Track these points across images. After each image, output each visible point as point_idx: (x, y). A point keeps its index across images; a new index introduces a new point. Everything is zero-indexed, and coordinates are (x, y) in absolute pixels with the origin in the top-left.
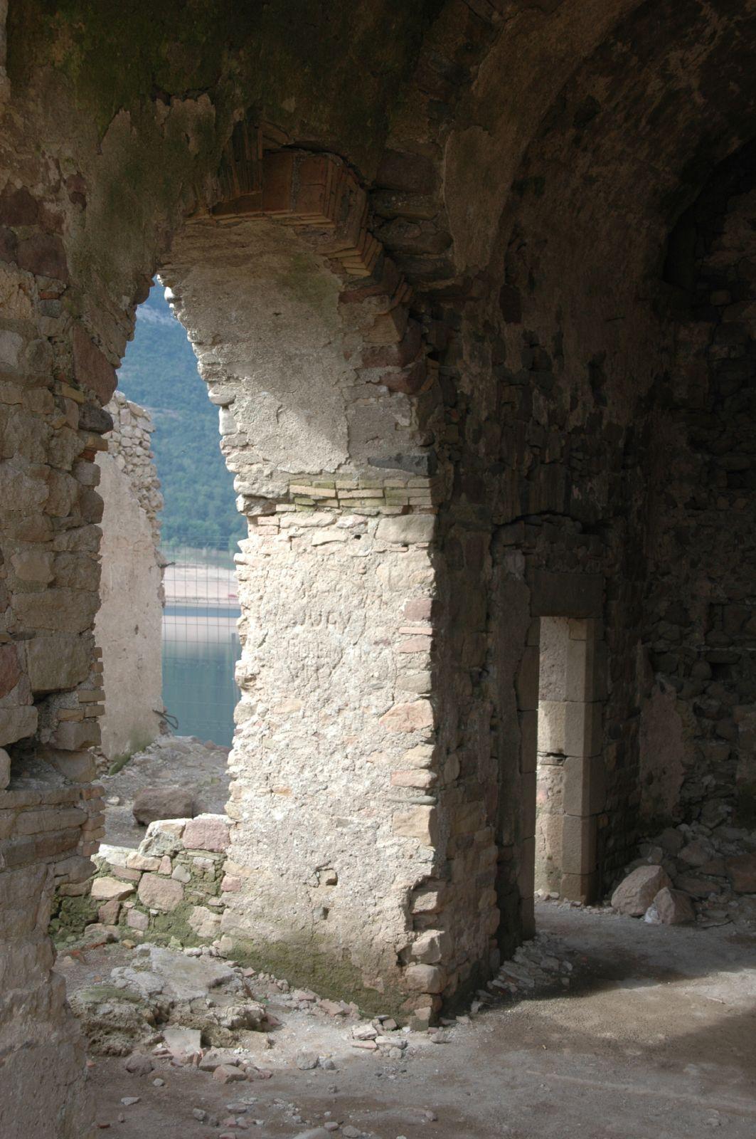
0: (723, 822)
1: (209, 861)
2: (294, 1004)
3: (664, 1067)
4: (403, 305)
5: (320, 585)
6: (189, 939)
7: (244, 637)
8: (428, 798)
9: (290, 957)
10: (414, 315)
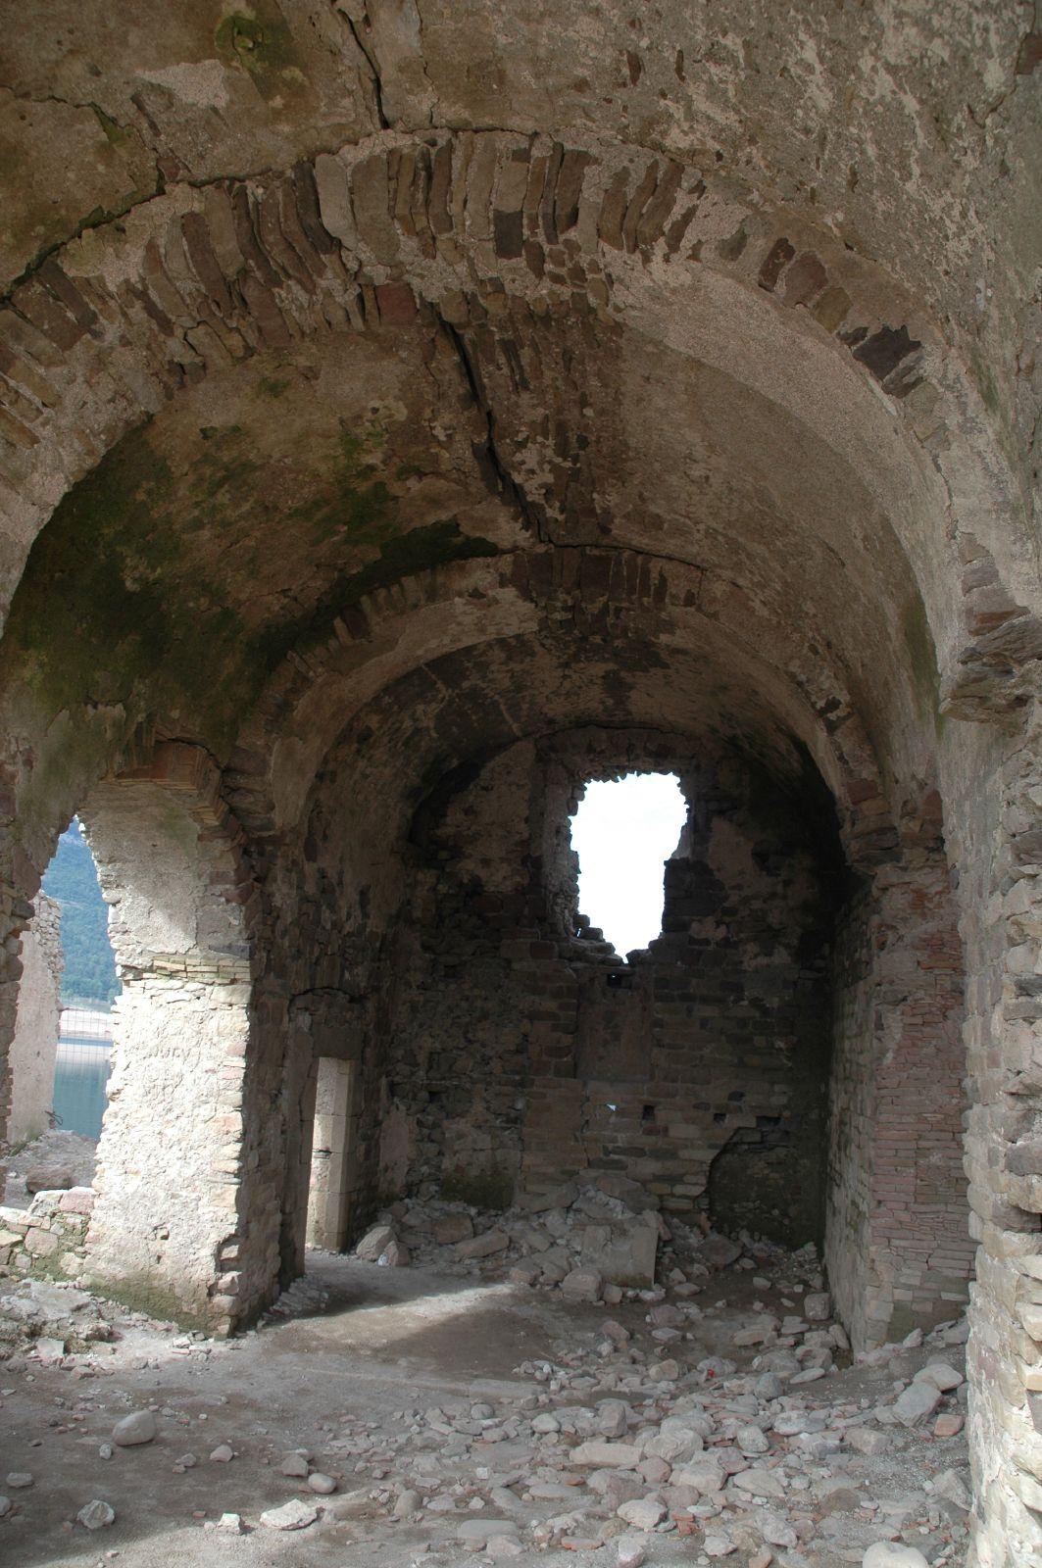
0: (433, 1197)
1: (78, 1221)
2: (132, 1323)
3: (384, 1361)
4: (240, 845)
5: (170, 1030)
6: (60, 1276)
7: (114, 1063)
8: (236, 1180)
9: (132, 1289)
10: (246, 852)
